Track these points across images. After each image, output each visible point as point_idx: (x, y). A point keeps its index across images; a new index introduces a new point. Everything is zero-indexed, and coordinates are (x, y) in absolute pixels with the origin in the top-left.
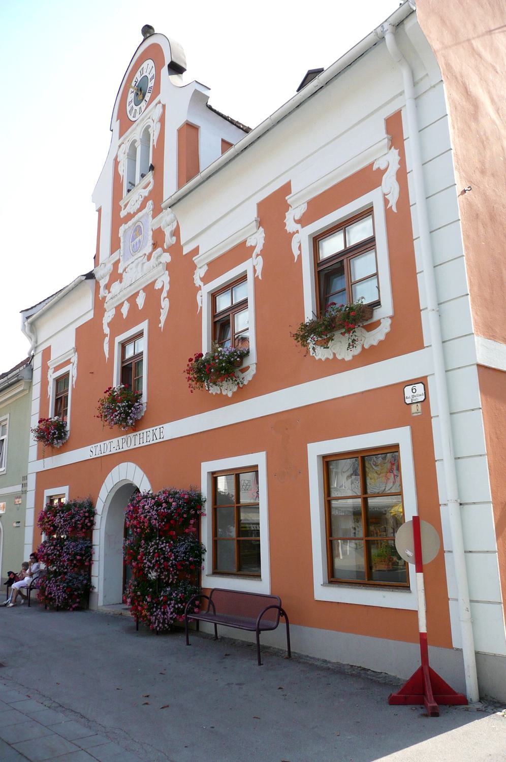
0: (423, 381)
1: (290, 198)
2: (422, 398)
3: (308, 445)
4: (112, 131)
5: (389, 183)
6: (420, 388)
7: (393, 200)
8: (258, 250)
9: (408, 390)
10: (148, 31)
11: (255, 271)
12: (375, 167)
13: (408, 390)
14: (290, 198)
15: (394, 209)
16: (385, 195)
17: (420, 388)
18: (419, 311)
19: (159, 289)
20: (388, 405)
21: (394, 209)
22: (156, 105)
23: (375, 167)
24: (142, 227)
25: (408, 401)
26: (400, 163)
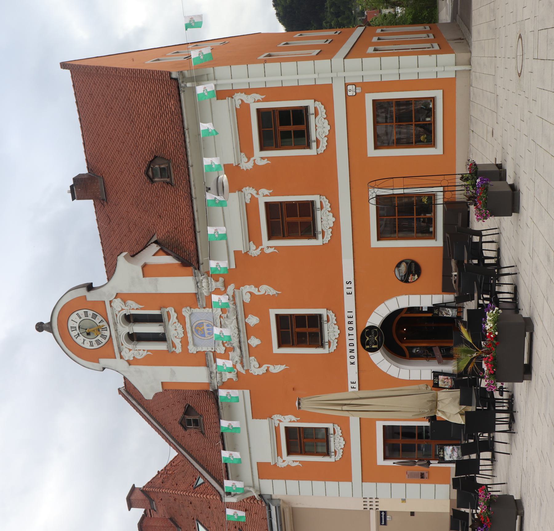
0: (346, 85)
1: (361, 398)
2: (354, 86)
3: (369, 156)
4: (104, 369)
5: (249, 99)
6: (349, 87)
7: (258, 97)
8: (254, 192)
9: (350, 94)
10: (40, 327)
11: (267, 196)
12: (238, 107)
13: (350, 94)
14: (361, 398)
15: (263, 97)
16: (255, 102)
17: (349, 87)
18: (299, 87)
19: (250, 298)
20: (353, 104)
21: (263, 97)
22: (111, 306)
23: (238, 107)
24: (197, 323)
25: (354, 94)
26: (242, 93)
